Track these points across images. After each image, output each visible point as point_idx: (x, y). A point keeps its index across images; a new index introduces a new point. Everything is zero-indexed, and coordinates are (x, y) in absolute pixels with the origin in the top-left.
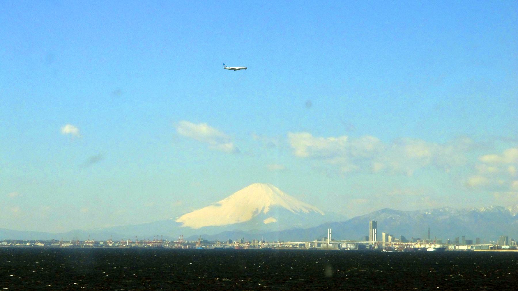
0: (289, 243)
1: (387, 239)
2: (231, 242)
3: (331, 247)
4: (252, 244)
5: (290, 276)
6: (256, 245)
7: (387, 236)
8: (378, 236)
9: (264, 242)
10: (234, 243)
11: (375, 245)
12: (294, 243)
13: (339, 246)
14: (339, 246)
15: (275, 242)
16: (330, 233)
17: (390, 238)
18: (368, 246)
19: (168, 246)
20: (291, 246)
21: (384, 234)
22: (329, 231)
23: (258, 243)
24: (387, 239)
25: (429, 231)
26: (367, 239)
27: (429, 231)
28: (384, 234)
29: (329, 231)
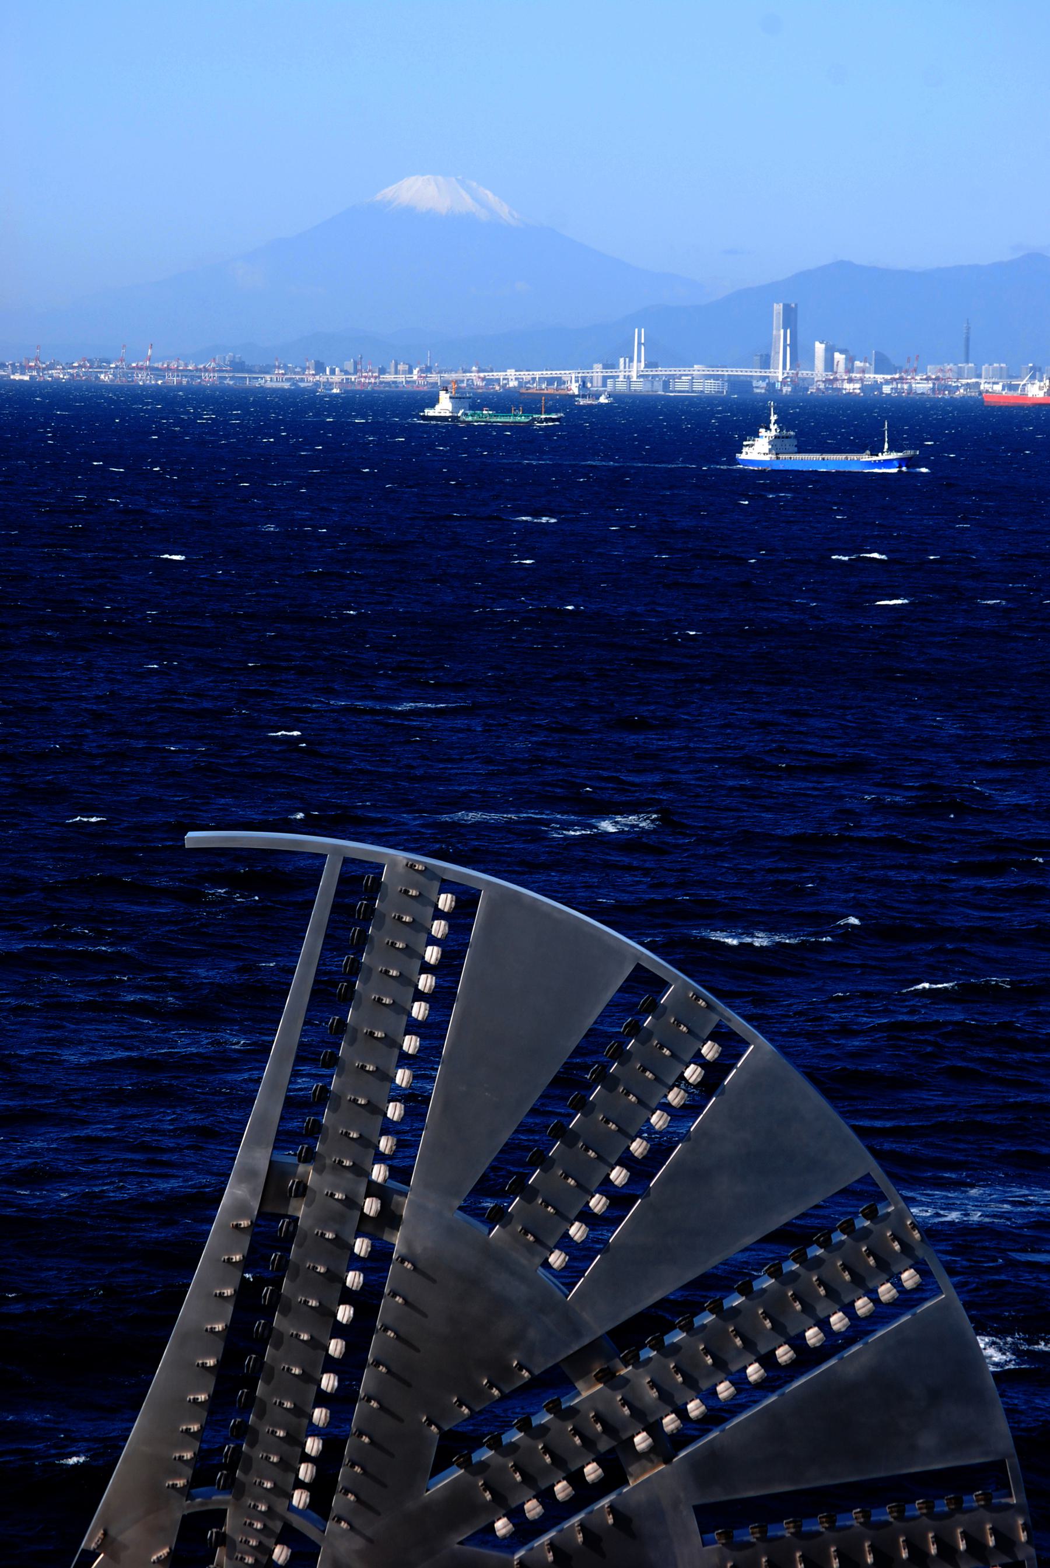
0: (511, 373)
1: (829, 364)
2: (320, 368)
3: (639, 386)
4: (388, 378)
5: (916, 696)
6: (401, 378)
7: (830, 352)
8: (799, 354)
9: (428, 370)
10: (333, 372)
11: (784, 383)
12: (526, 375)
13: (666, 385)
14: (666, 385)
15: (465, 372)
16: (639, 344)
17: (839, 357)
18: (764, 384)
19: (235, 384)
20: (513, 384)
21: (820, 348)
22: (639, 335)
23: (411, 372)
24: (829, 364)
25: (968, 339)
26: (766, 362)
27: (968, 339)
28: (820, 348)
29: (639, 335)
